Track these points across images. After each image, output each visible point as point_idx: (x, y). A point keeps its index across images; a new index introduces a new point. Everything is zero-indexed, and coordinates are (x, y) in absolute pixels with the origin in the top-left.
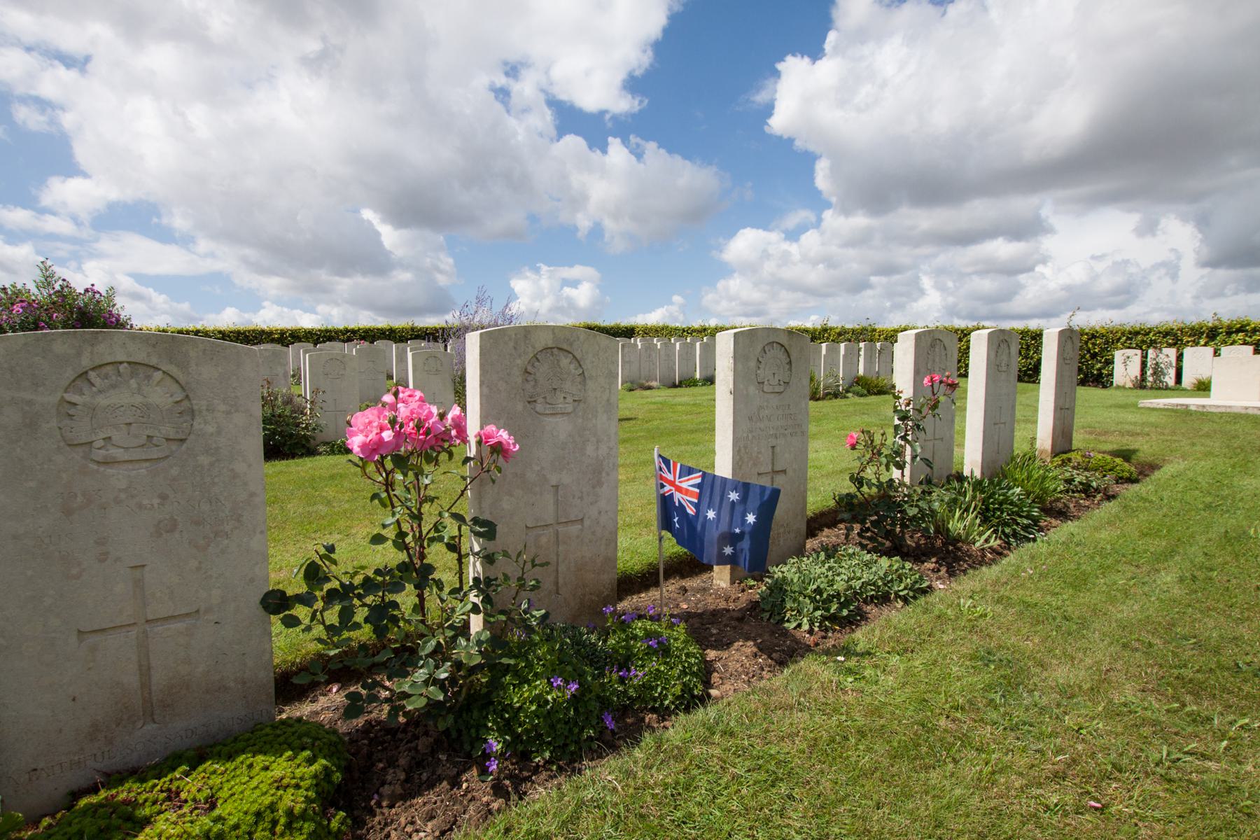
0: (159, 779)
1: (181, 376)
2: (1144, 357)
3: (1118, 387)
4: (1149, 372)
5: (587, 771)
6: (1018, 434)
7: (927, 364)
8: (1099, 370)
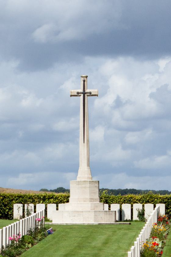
2: (24, 206)
4: (25, 214)
8: (8, 212)
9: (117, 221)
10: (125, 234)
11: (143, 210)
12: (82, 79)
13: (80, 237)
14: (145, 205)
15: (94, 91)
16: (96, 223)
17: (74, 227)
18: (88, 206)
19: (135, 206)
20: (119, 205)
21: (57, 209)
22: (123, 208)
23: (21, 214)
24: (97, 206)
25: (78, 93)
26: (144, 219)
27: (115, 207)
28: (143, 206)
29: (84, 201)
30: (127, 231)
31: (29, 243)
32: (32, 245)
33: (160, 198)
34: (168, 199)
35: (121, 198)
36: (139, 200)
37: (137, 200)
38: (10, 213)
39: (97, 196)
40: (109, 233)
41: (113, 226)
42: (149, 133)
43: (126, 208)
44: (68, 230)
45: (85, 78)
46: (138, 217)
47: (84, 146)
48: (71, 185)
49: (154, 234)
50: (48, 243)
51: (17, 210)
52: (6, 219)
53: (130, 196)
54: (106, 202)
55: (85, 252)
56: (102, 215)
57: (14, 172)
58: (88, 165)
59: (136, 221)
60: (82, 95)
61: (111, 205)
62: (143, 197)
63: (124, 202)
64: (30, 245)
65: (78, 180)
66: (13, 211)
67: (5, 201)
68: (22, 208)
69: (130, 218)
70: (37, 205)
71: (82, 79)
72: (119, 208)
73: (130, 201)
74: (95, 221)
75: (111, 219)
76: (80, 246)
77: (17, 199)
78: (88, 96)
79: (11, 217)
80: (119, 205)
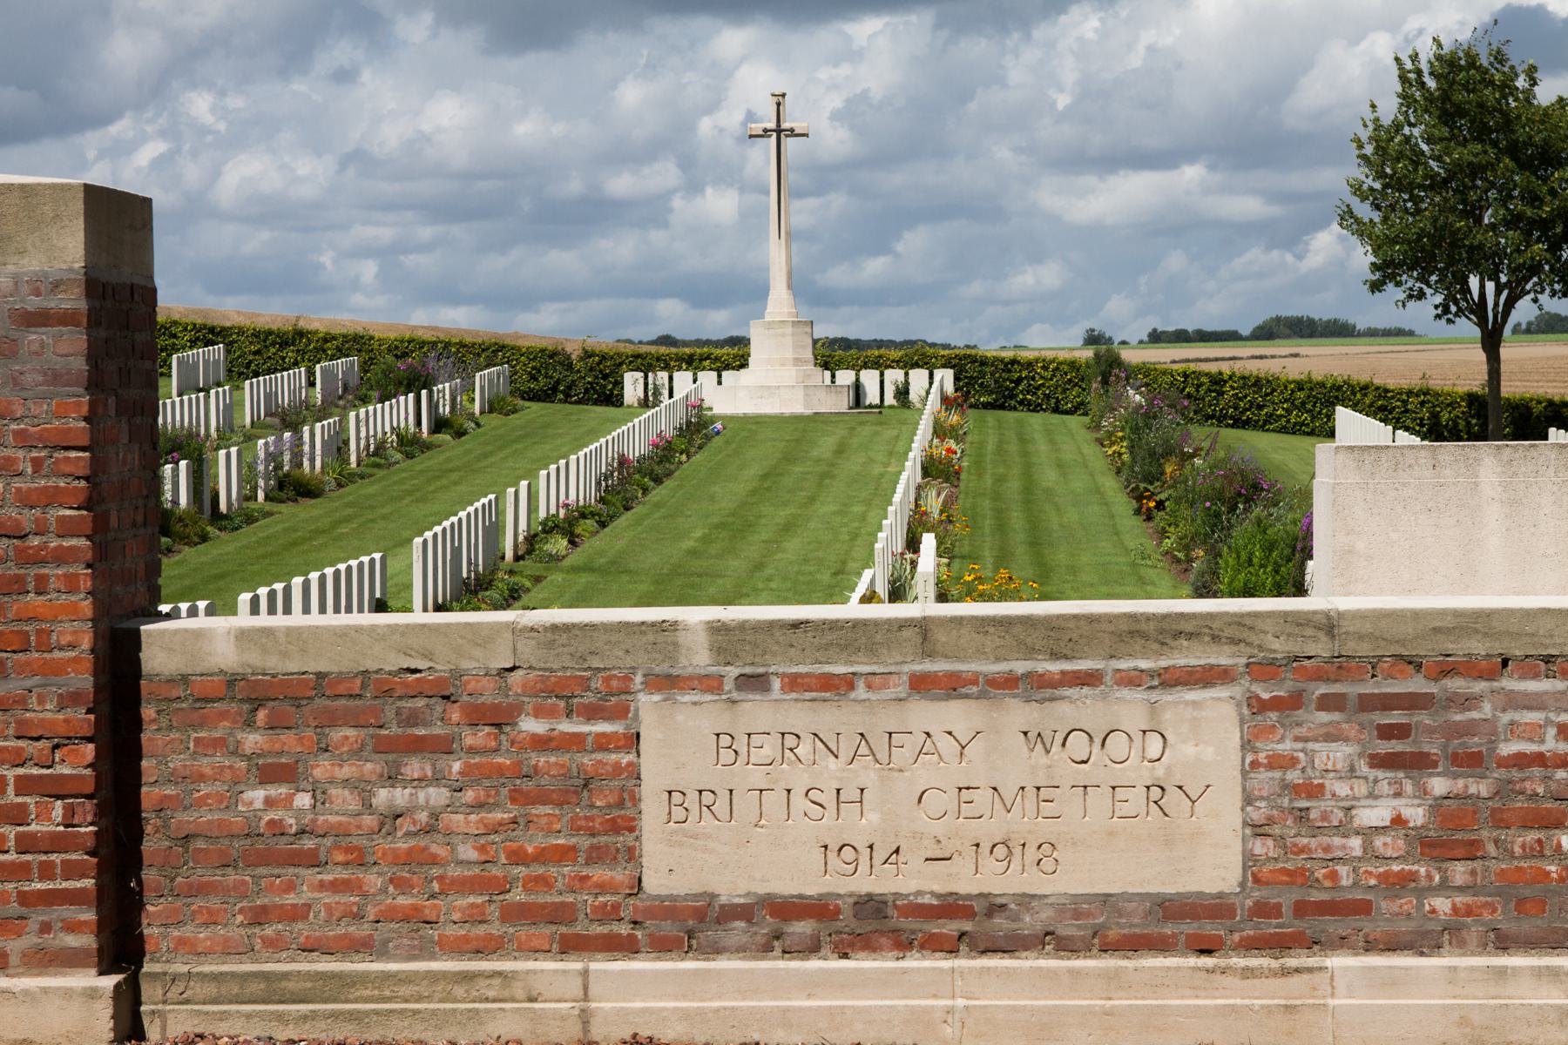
1: (1108, 678)
2: (646, 377)
3: (629, 406)
4: (650, 394)
8: (611, 390)
9: (850, 408)
10: (876, 433)
11: (907, 383)
12: (775, 99)
13: (781, 441)
14: (910, 372)
15: (799, 127)
16: (809, 412)
17: (767, 419)
18: (789, 374)
19: (888, 373)
20: (853, 373)
21: (720, 383)
22: (862, 379)
23: (642, 395)
24: (809, 375)
25: (766, 130)
26: (909, 402)
27: (845, 377)
28: (907, 374)
29: (782, 365)
30: (879, 428)
31: (681, 454)
32: (689, 457)
33: (943, 356)
34: (960, 359)
35: (858, 359)
36: (897, 362)
37: (893, 361)
38: (616, 392)
39: (809, 354)
40: (841, 432)
41: (846, 418)
42: (838, 201)
43: (870, 378)
44: (754, 427)
45: (780, 98)
46: (895, 397)
47: (780, 245)
48: (752, 330)
49: (940, 431)
50: (720, 452)
51: (633, 388)
52: (607, 405)
53: (876, 353)
54: (826, 366)
55: (801, 469)
56: (821, 394)
57: (528, 299)
58: (789, 287)
59: (891, 407)
60: (775, 134)
61: (837, 373)
62: (907, 356)
63: (865, 366)
64: (684, 457)
65: (768, 318)
66: (622, 388)
67: (605, 367)
68: (641, 381)
69: (877, 401)
70: (676, 375)
71: (775, 99)
72: (854, 379)
73: (879, 364)
74: (806, 405)
75: (840, 403)
76: (789, 458)
77: (631, 362)
78: (787, 136)
79: (618, 401)
80: (853, 373)
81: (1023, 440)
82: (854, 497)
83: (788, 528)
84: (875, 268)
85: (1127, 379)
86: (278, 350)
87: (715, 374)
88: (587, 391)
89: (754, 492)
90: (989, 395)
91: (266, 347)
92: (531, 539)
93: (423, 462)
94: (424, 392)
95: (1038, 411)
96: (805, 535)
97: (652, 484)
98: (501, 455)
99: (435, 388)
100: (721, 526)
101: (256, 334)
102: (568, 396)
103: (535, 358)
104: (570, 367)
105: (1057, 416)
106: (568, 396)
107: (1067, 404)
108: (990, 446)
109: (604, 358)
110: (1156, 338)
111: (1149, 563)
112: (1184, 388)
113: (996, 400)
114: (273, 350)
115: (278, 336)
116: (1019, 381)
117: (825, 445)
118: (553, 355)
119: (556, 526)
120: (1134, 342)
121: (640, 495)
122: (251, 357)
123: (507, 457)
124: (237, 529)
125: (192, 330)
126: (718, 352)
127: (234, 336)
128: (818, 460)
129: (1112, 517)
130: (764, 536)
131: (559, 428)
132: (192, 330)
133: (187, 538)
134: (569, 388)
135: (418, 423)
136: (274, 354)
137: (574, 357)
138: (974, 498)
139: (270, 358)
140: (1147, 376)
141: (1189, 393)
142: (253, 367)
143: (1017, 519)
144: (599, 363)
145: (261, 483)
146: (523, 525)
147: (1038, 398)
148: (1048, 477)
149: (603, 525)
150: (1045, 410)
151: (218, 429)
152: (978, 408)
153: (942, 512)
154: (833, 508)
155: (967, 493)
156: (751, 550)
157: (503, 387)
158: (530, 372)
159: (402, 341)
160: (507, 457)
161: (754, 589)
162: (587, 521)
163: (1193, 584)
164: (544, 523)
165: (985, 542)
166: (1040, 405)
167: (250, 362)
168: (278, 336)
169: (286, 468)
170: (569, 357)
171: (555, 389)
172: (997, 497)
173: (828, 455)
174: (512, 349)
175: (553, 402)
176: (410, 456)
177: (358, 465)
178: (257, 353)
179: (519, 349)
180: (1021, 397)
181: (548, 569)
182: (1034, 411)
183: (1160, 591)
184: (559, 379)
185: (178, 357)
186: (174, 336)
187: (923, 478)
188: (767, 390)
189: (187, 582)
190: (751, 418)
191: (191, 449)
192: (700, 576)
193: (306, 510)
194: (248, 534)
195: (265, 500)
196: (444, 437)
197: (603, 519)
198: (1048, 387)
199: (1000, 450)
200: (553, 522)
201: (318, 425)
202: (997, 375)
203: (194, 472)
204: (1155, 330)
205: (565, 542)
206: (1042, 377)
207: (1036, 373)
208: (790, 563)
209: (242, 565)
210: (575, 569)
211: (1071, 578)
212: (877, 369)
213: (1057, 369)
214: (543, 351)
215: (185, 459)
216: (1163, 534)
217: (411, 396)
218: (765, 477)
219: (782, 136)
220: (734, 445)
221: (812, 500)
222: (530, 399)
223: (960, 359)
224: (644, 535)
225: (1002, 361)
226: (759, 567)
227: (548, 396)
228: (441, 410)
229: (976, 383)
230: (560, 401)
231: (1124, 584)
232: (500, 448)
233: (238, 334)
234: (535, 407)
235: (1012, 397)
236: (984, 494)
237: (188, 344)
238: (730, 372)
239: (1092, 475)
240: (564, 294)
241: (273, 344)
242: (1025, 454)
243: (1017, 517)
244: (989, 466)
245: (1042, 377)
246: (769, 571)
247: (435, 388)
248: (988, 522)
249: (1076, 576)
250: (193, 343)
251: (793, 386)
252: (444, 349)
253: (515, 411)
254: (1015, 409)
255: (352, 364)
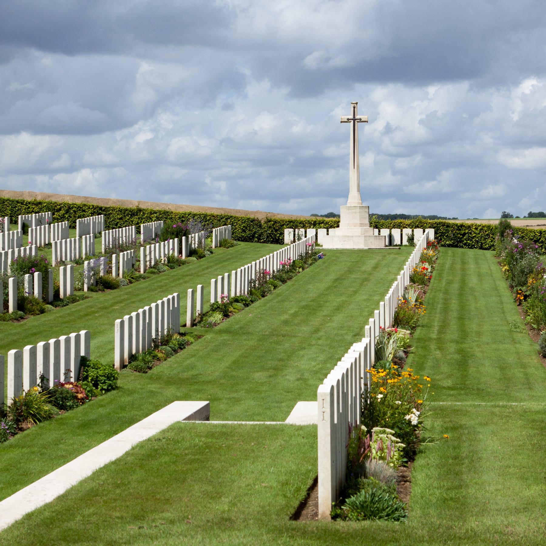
0: (403, 269)
2: (294, 231)
4: (296, 239)
5: (283, 471)
6: (181, 319)
7: (173, 287)
8: (279, 237)
10: (395, 259)
11: (413, 235)
12: (353, 105)
15: (364, 118)
16: (366, 248)
17: (345, 251)
18: (358, 231)
21: (328, 234)
22: (392, 233)
24: (367, 231)
25: (348, 119)
26: (414, 243)
27: (385, 232)
28: (413, 231)
30: (397, 256)
31: (299, 268)
32: (303, 269)
33: (430, 223)
34: (438, 224)
35: (391, 224)
36: (409, 225)
37: (407, 225)
39: (367, 221)
40: (379, 257)
41: (383, 251)
43: (396, 233)
44: (338, 255)
45: (355, 105)
47: (354, 172)
48: (341, 210)
49: (424, 259)
52: (277, 244)
53: (399, 221)
54: (376, 227)
55: (355, 276)
56: (372, 240)
57: (285, 198)
58: (359, 190)
59: (406, 246)
60: (352, 121)
63: (394, 227)
64: (301, 270)
65: (348, 205)
67: (276, 226)
68: (292, 233)
69: (399, 243)
70: (308, 230)
71: (353, 105)
72: (389, 233)
73: (400, 226)
74: (365, 246)
75: (380, 244)
76: (350, 271)
77: (288, 224)
78: (358, 122)
79: (282, 242)
81: (464, 263)
82: (376, 291)
83: (338, 309)
84: (429, 186)
85: (513, 234)
86: (130, 218)
87: (326, 230)
88: (268, 237)
89: (328, 288)
90: (450, 241)
91: (125, 216)
92: (203, 315)
93: (179, 271)
94: (184, 238)
95: (473, 248)
96: (346, 312)
97: (281, 283)
98: (215, 268)
99: (190, 236)
100: (305, 307)
101: (120, 211)
102: (259, 239)
103: (245, 222)
104: (260, 226)
105: (481, 250)
106: (259, 239)
107: (486, 245)
108: (447, 266)
109: (275, 222)
110: (532, 215)
111: (518, 330)
112: (540, 239)
113: (454, 243)
114: (128, 218)
115: (130, 211)
116: (464, 234)
117: (370, 264)
118: (253, 221)
119: (218, 307)
120: (522, 217)
121: (272, 289)
122: (118, 221)
123: (217, 269)
124: (65, 306)
125: (92, 209)
126: (327, 219)
127: (111, 211)
128: (364, 272)
129: (502, 303)
130: (325, 313)
131: (248, 255)
132: (92, 209)
133: (33, 311)
134: (260, 236)
135: (180, 252)
136: (128, 219)
137: (262, 222)
138: (435, 292)
139: (126, 221)
140: (522, 233)
141: (542, 240)
142: (119, 225)
143: (454, 304)
144: (273, 225)
145: (86, 281)
146: (198, 308)
147: (473, 242)
148: (473, 281)
149: (247, 305)
150: (476, 248)
151: (86, 254)
152: (445, 247)
153: (416, 301)
154: (365, 297)
155: (432, 290)
156: (315, 321)
157: (228, 236)
158: (242, 229)
159: (186, 214)
160: (217, 269)
161: (310, 345)
162: (238, 304)
163: (540, 345)
164: (212, 306)
165: (436, 317)
166: (474, 245)
167: (118, 223)
168: (130, 211)
169: (102, 274)
170: (260, 222)
171: (253, 236)
172: (446, 292)
173: (370, 269)
174: (235, 218)
175: (253, 242)
176: (172, 268)
177: (144, 272)
178: (121, 219)
179: (238, 218)
180: (465, 241)
181: (207, 331)
182: (471, 248)
183: (523, 347)
184: (255, 232)
185: (79, 220)
186: (84, 211)
187: (410, 283)
188: (348, 238)
189: (15, 338)
190: (339, 250)
191: (42, 266)
192: (284, 336)
193: (109, 295)
194: (72, 307)
195: (88, 291)
196: (193, 259)
197: (247, 303)
198: (478, 237)
199: (452, 268)
200: (217, 305)
201: (121, 254)
202: (454, 232)
203: (43, 278)
204: (531, 212)
205: (220, 316)
206: (475, 233)
207: (472, 231)
208: (334, 329)
209: (51, 327)
210: (221, 332)
211: (477, 339)
212: (400, 228)
213: (482, 229)
214: (248, 219)
215: (37, 271)
216: (526, 313)
217: (176, 239)
218: (336, 280)
219: (356, 122)
220: (326, 265)
221: (355, 292)
222: (242, 241)
223: (438, 224)
224: (265, 312)
225: (457, 225)
226: (317, 330)
227: (250, 239)
228: (193, 246)
229: (444, 235)
230: (256, 241)
231: (505, 343)
232: (216, 264)
233: (112, 210)
234: (242, 244)
235: (461, 242)
236: (440, 290)
237: (90, 215)
238: (333, 229)
239: (494, 281)
240: (301, 195)
241: (128, 215)
242: (463, 269)
243: (455, 303)
244: (445, 276)
245: (475, 233)
246: (321, 334)
247: (190, 236)
248: (439, 306)
249: (479, 338)
250: (93, 214)
251: (359, 236)
252: (204, 218)
253: (232, 246)
254: (462, 247)
255: (160, 224)
